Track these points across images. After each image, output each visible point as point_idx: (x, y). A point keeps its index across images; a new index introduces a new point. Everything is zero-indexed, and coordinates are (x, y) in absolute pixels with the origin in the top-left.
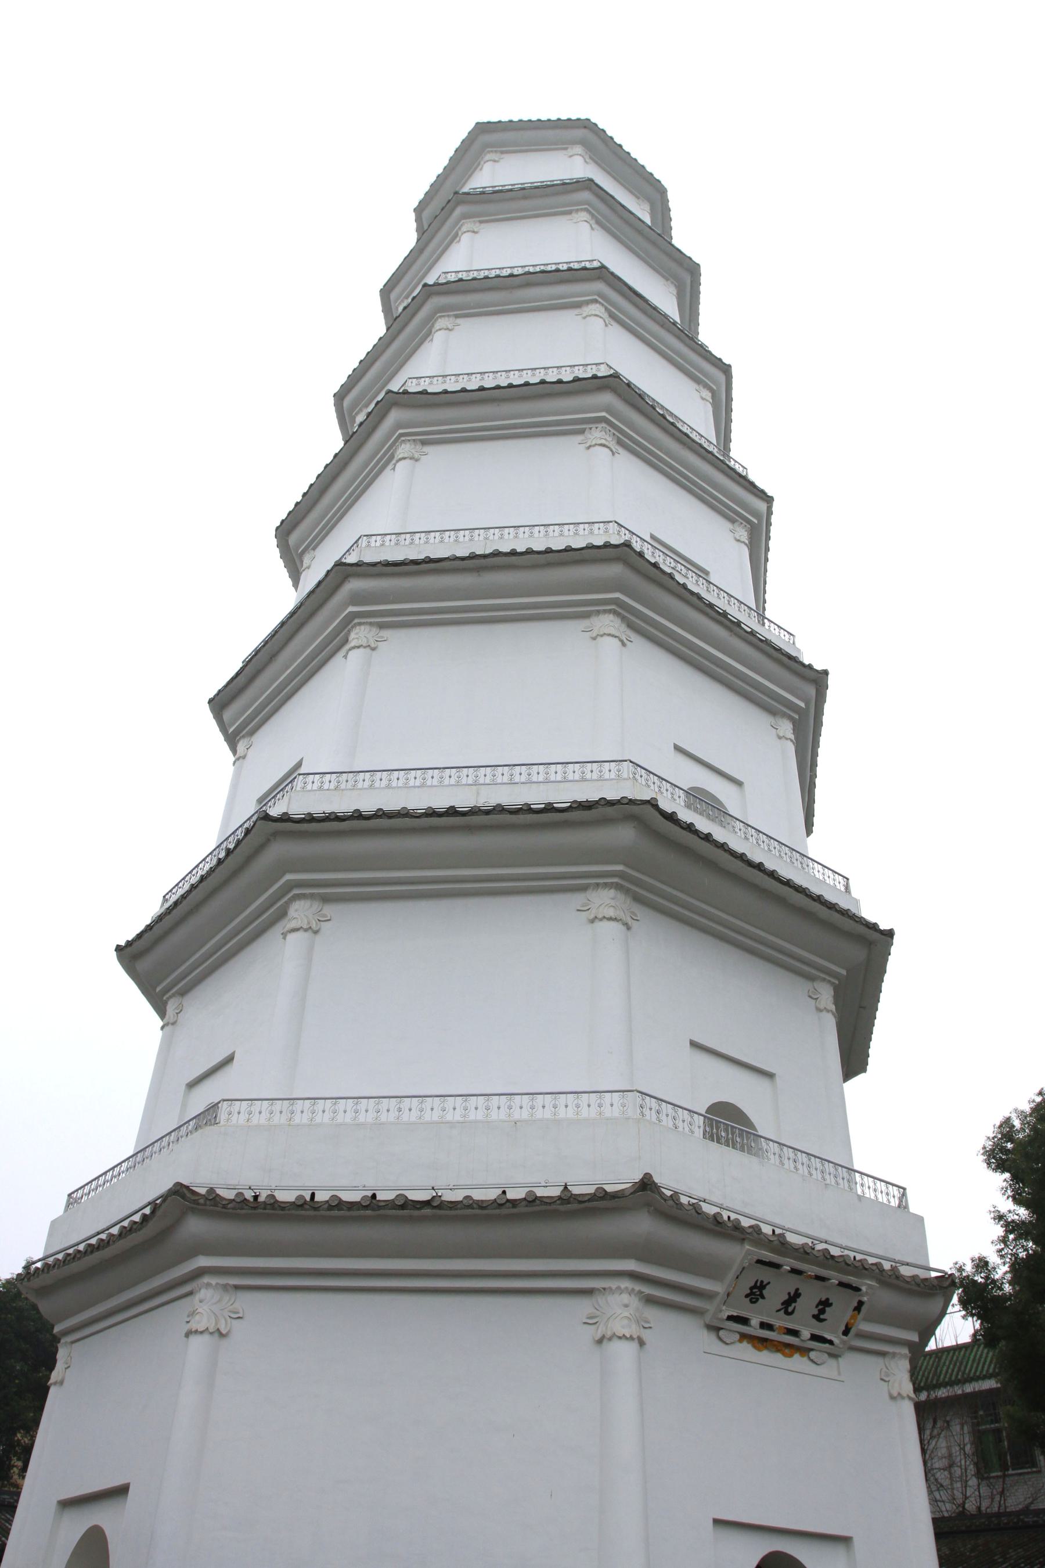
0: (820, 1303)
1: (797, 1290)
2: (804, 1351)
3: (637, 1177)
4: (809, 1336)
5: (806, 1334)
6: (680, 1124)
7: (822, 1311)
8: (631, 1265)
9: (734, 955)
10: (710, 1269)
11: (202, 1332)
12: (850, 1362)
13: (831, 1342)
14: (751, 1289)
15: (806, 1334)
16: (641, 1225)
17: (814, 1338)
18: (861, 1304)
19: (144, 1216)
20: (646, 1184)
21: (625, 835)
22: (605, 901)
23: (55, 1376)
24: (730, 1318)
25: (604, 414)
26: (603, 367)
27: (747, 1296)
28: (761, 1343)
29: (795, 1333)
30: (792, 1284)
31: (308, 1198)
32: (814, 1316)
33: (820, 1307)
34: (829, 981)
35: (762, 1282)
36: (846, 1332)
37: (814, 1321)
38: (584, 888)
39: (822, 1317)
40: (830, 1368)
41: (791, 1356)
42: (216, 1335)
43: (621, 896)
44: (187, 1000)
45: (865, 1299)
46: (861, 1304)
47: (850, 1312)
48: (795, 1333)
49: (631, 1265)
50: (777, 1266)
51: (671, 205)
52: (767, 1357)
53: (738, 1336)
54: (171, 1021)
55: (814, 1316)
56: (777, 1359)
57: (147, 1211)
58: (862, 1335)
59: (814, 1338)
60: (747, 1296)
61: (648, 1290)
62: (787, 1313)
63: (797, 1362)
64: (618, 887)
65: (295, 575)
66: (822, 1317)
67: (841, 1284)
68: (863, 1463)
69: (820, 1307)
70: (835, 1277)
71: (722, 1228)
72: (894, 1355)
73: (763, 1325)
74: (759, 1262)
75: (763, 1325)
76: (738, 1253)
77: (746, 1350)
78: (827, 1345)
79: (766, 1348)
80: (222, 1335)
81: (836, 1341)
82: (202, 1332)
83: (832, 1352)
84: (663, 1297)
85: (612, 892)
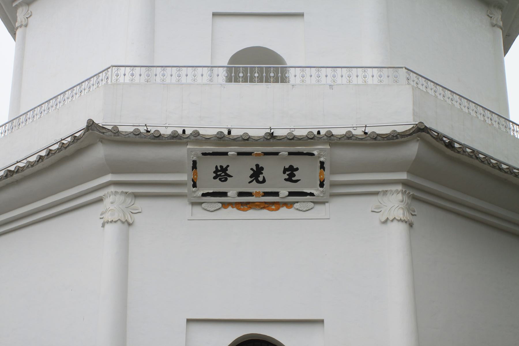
1: (257, 166)
2: (289, 205)
3: (84, 125)
4: (287, 193)
5: (284, 193)
7: (292, 175)
8: (109, 178)
10: (172, 167)
11: (115, 222)
13: (312, 194)
15: (284, 193)
17: (291, 194)
19: (41, 157)
27: (215, 178)
29: (276, 194)
30: (251, 163)
33: (288, 173)
35: (221, 167)
36: (322, 185)
37: (289, 183)
39: (294, 179)
40: (319, 211)
42: (126, 223)
44: (33, 8)
45: (322, 159)
47: (318, 170)
48: (276, 194)
49: (109, 178)
50: (226, 154)
52: (252, 213)
53: (220, 205)
54: (24, 23)
57: (43, 153)
58: (334, 185)
59: (291, 194)
60: (215, 178)
61: (130, 190)
62: (258, 182)
63: (283, 211)
66: (294, 179)
68: (361, 276)
69: (288, 173)
70: (284, 150)
71: (176, 139)
73: (241, 194)
74: (204, 154)
75: (241, 194)
77: (232, 212)
78: (308, 197)
79: (250, 208)
80: (130, 224)
81: (315, 193)
82: (115, 222)
83: (315, 201)
84: (140, 192)
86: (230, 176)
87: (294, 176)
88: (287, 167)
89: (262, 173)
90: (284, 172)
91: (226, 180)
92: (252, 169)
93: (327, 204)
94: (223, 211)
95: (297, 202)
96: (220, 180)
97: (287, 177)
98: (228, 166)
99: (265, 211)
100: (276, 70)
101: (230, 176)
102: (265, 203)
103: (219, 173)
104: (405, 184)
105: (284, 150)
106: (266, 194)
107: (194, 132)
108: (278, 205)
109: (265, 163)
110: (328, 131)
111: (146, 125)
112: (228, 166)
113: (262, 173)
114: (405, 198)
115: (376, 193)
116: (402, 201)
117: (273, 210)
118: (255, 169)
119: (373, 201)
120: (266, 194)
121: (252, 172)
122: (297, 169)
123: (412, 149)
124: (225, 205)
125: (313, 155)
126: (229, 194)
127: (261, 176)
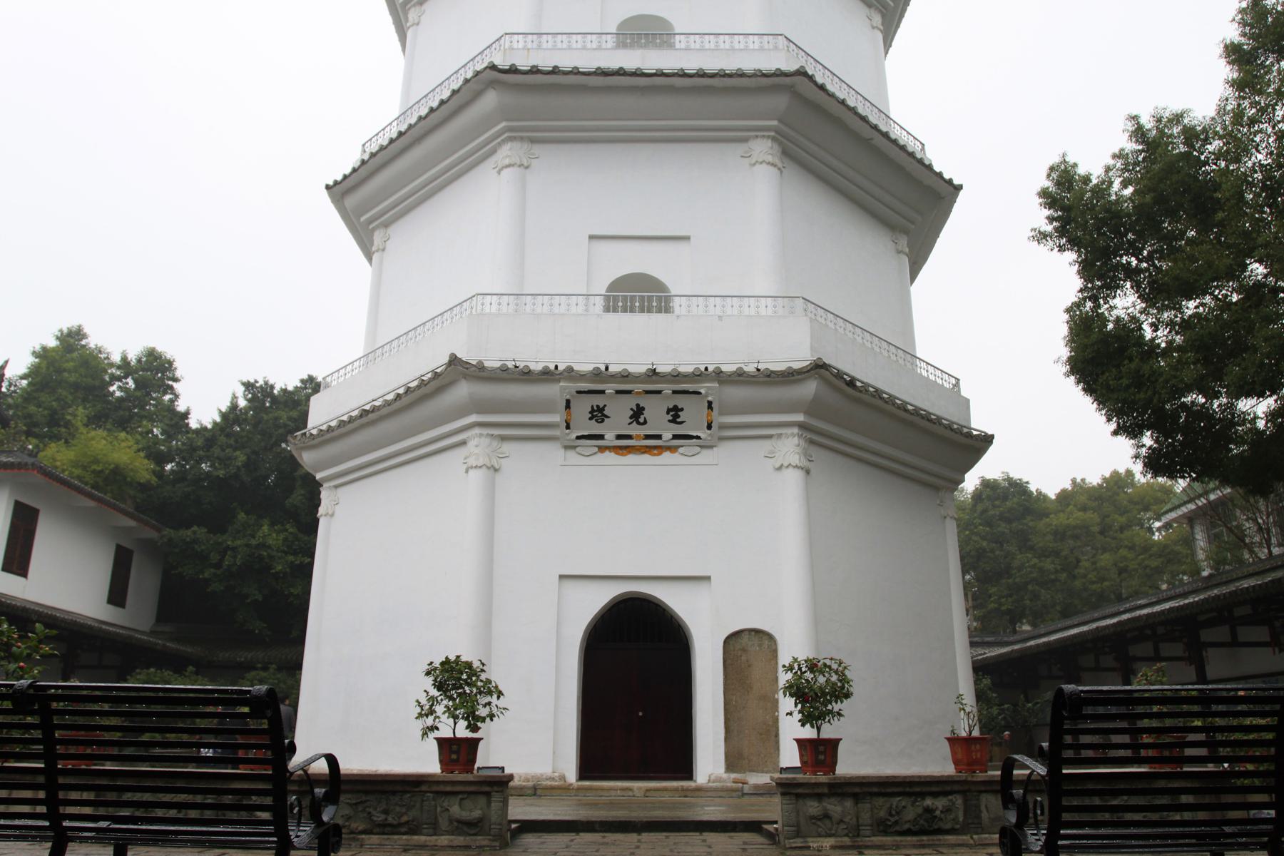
0: (669, 411)
2: (672, 449)
5: (667, 436)
7: (676, 416)
9: (646, 150)
12: (725, 452)
13: (698, 438)
15: (667, 436)
16: (463, 391)
17: (675, 437)
18: (710, 403)
20: (454, 360)
21: (490, 100)
22: (507, 152)
23: (321, 510)
24: (578, 438)
29: (659, 437)
30: (629, 403)
31: (603, 368)
34: (503, 141)
36: (709, 427)
37: (673, 425)
38: (745, 140)
40: (706, 456)
41: (660, 454)
43: (516, 145)
45: (710, 399)
46: (710, 403)
48: (659, 437)
50: (603, 392)
52: (632, 458)
56: (646, 458)
58: (723, 427)
59: (675, 437)
64: (511, 139)
72: (780, 436)
73: (619, 437)
74: (579, 392)
75: (619, 437)
76: (555, 392)
77: (610, 457)
81: (702, 436)
84: (510, 434)
85: (509, 145)
91: (603, 421)
99: (646, 456)
106: (648, 437)
108: (660, 449)
114: (802, 442)
120: (648, 437)
123: (810, 388)
124: (602, 449)
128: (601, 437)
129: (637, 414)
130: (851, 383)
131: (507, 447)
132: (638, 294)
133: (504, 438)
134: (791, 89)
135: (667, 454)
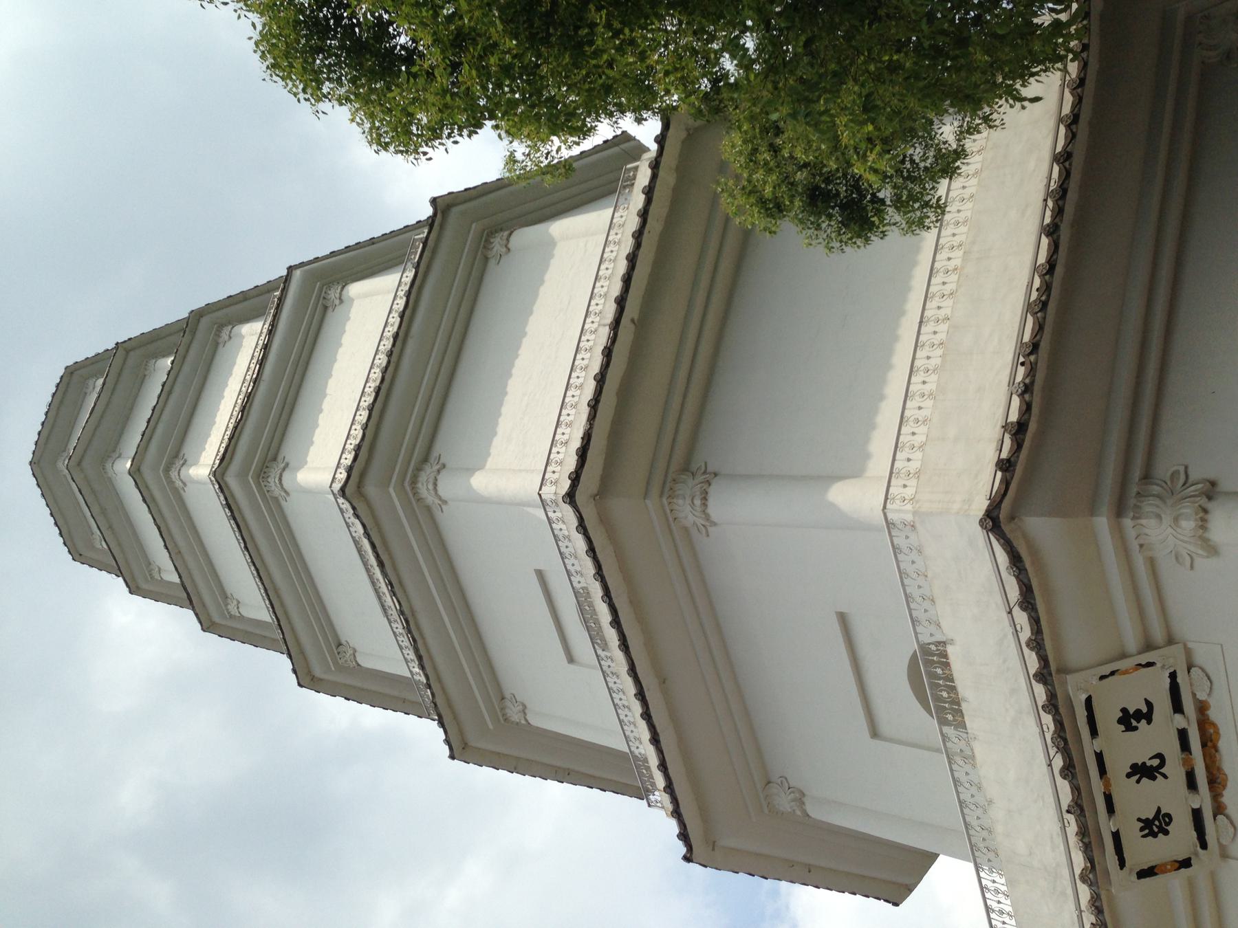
0: (1130, 728)
1: (1129, 776)
2: (1202, 708)
6: (968, 192)
7: (1138, 715)
12: (1186, 628)
14: (1155, 835)
15: (1180, 722)
17: (1178, 707)
25: (391, 490)
26: (227, 338)
27: (1166, 833)
28: (1216, 782)
29: (1183, 735)
32: (1149, 722)
33: (1134, 723)
35: (1142, 829)
37: (1156, 716)
39: (1145, 710)
41: (1214, 725)
48: (1183, 735)
50: (1116, 836)
51: (609, 795)
53: (1220, 817)
55: (1149, 722)
59: (1178, 707)
60: (1166, 833)
65: (641, 792)
66: (1145, 710)
67: (1094, 732)
69: (1134, 723)
73: (1192, 784)
75: (1192, 784)
78: (1179, 680)
79: (1219, 769)
86: (1159, 810)
87: (1138, 711)
88: (1123, 728)
89: (1144, 763)
90: (1136, 728)
91: (1169, 816)
92: (1138, 782)
93: (1190, 645)
94: (1231, 810)
95: (1194, 695)
96: (1168, 824)
97: (1144, 722)
98: (1139, 820)
99: (1222, 744)
100: (928, 663)
101: (1159, 810)
102: (1204, 745)
103: (1156, 830)
104: (1120, 510)
105: (1090, 747)
106: (1185, 745)
107: (1038, 681)
108: (1205, 724)
109: (1118, 766)
110: (1028, 646)
111: (1010, 612)
112: (1139, 820)
113: (1144, 763)
114: (1149, 506)
115: (1152, 563)
116: (1159, 517)
117: (1217, 732)
118: (1137, 777)
119: (1167, 568)
120: (1185, 745)
121: (1144, 780)
122: (1124, 710)
123: (1041, 528)
124: (1219, 809)
125: (1089, 701)
126: (1196, 806)
127: (1149, 763)
128: (1197, 815)
129: (1142, 771)
130: (1018, 430)
131: (1165, 467)
132: (931, 635)
133: (1147, 477)
134: (603, 492)
135: (1213, 714)
